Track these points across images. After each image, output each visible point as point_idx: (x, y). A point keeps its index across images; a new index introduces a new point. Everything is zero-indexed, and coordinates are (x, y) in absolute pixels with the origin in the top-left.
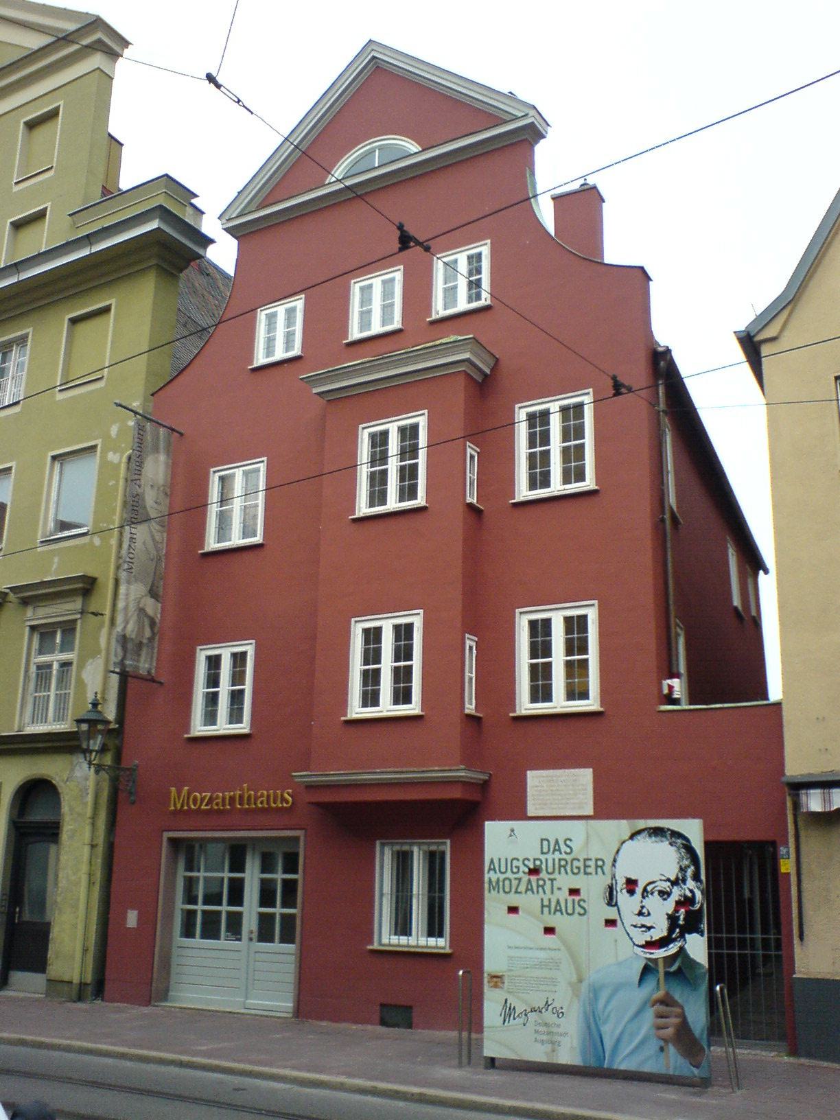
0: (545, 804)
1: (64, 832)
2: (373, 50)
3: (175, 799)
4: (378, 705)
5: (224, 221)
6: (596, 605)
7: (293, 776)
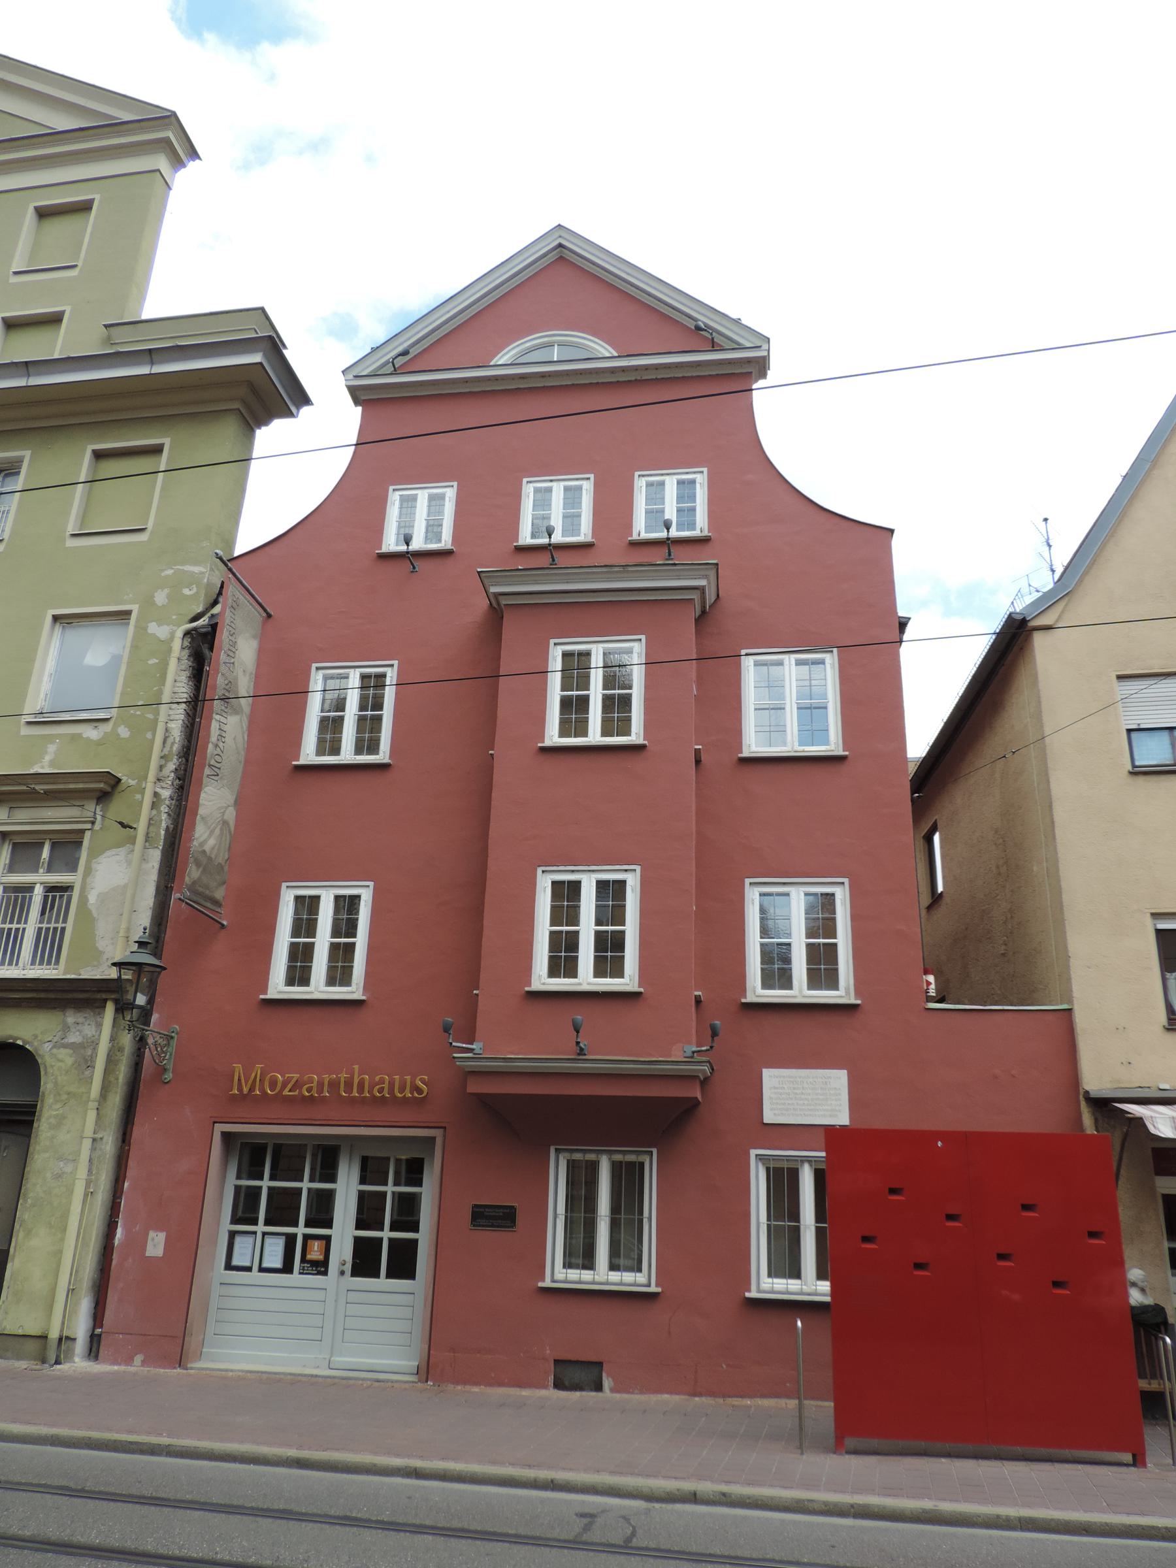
0: (787, 1110)
1: (43, 1120)
2: (560, 237)
3: (239, 1080)
4: (575, 976)
5: (351, 377)
6: (372, 887)
7: (454, 1058)
